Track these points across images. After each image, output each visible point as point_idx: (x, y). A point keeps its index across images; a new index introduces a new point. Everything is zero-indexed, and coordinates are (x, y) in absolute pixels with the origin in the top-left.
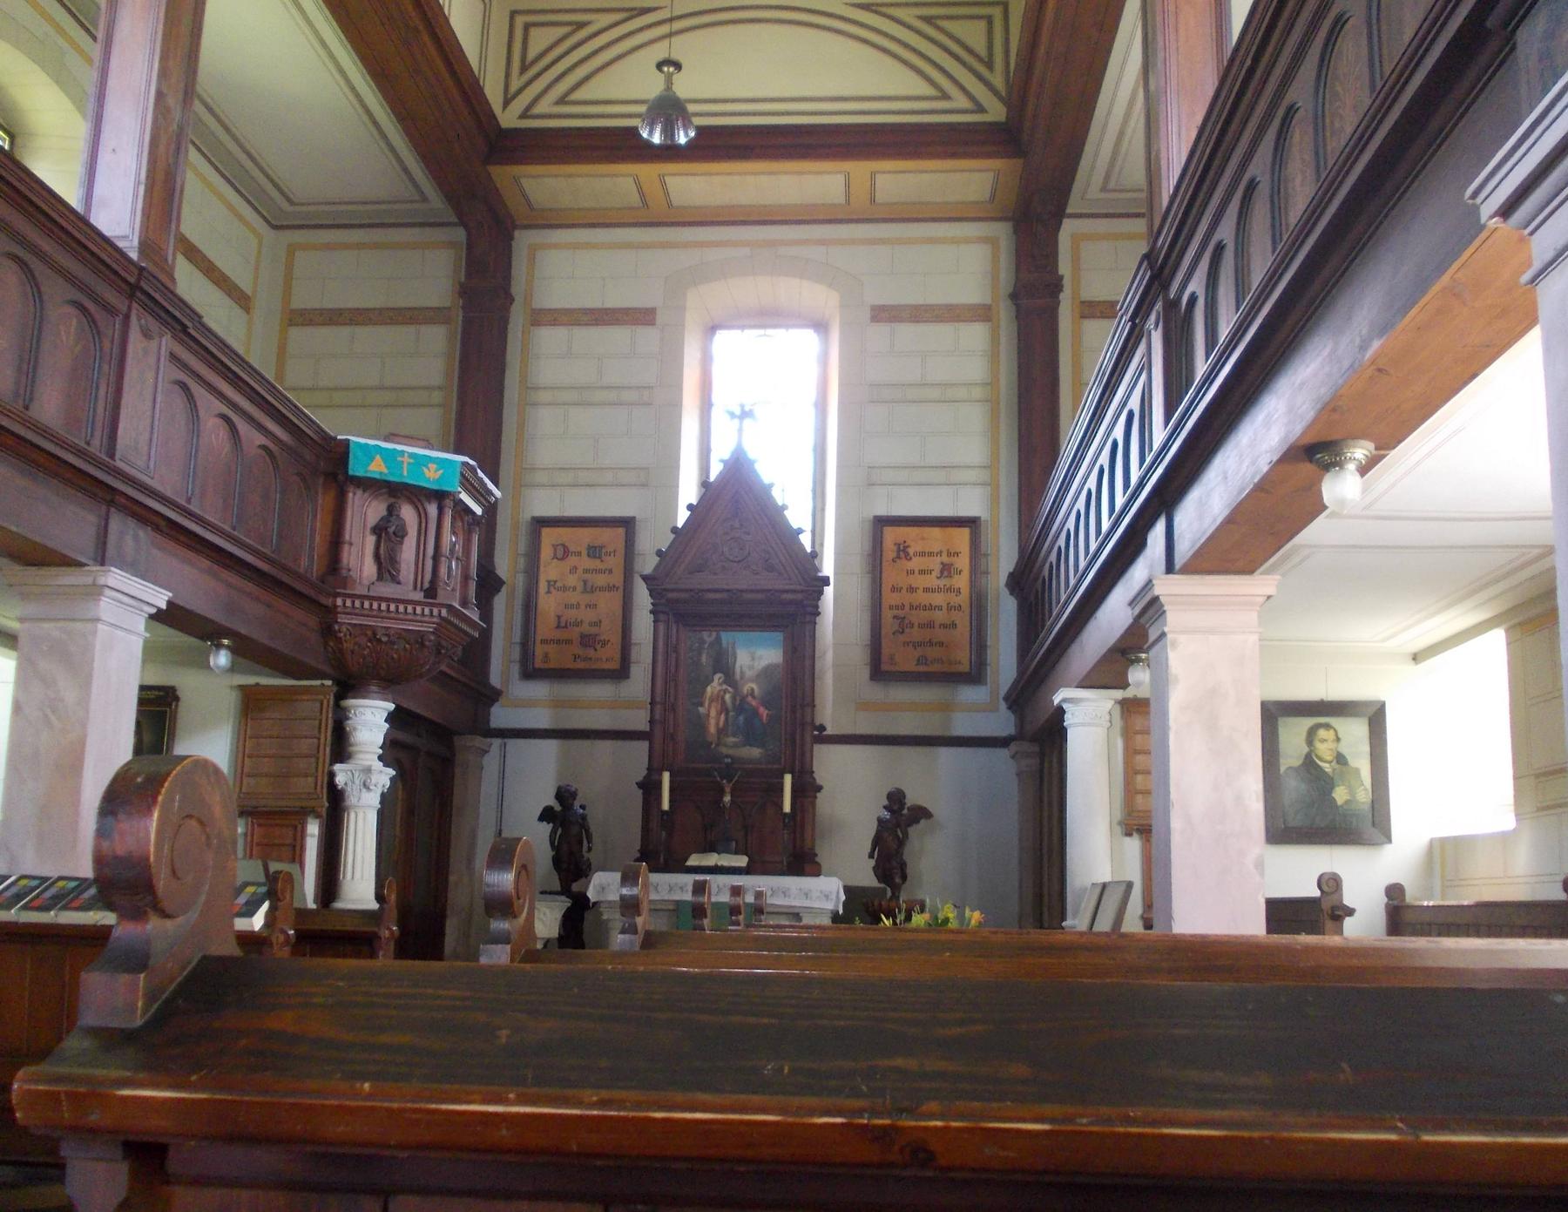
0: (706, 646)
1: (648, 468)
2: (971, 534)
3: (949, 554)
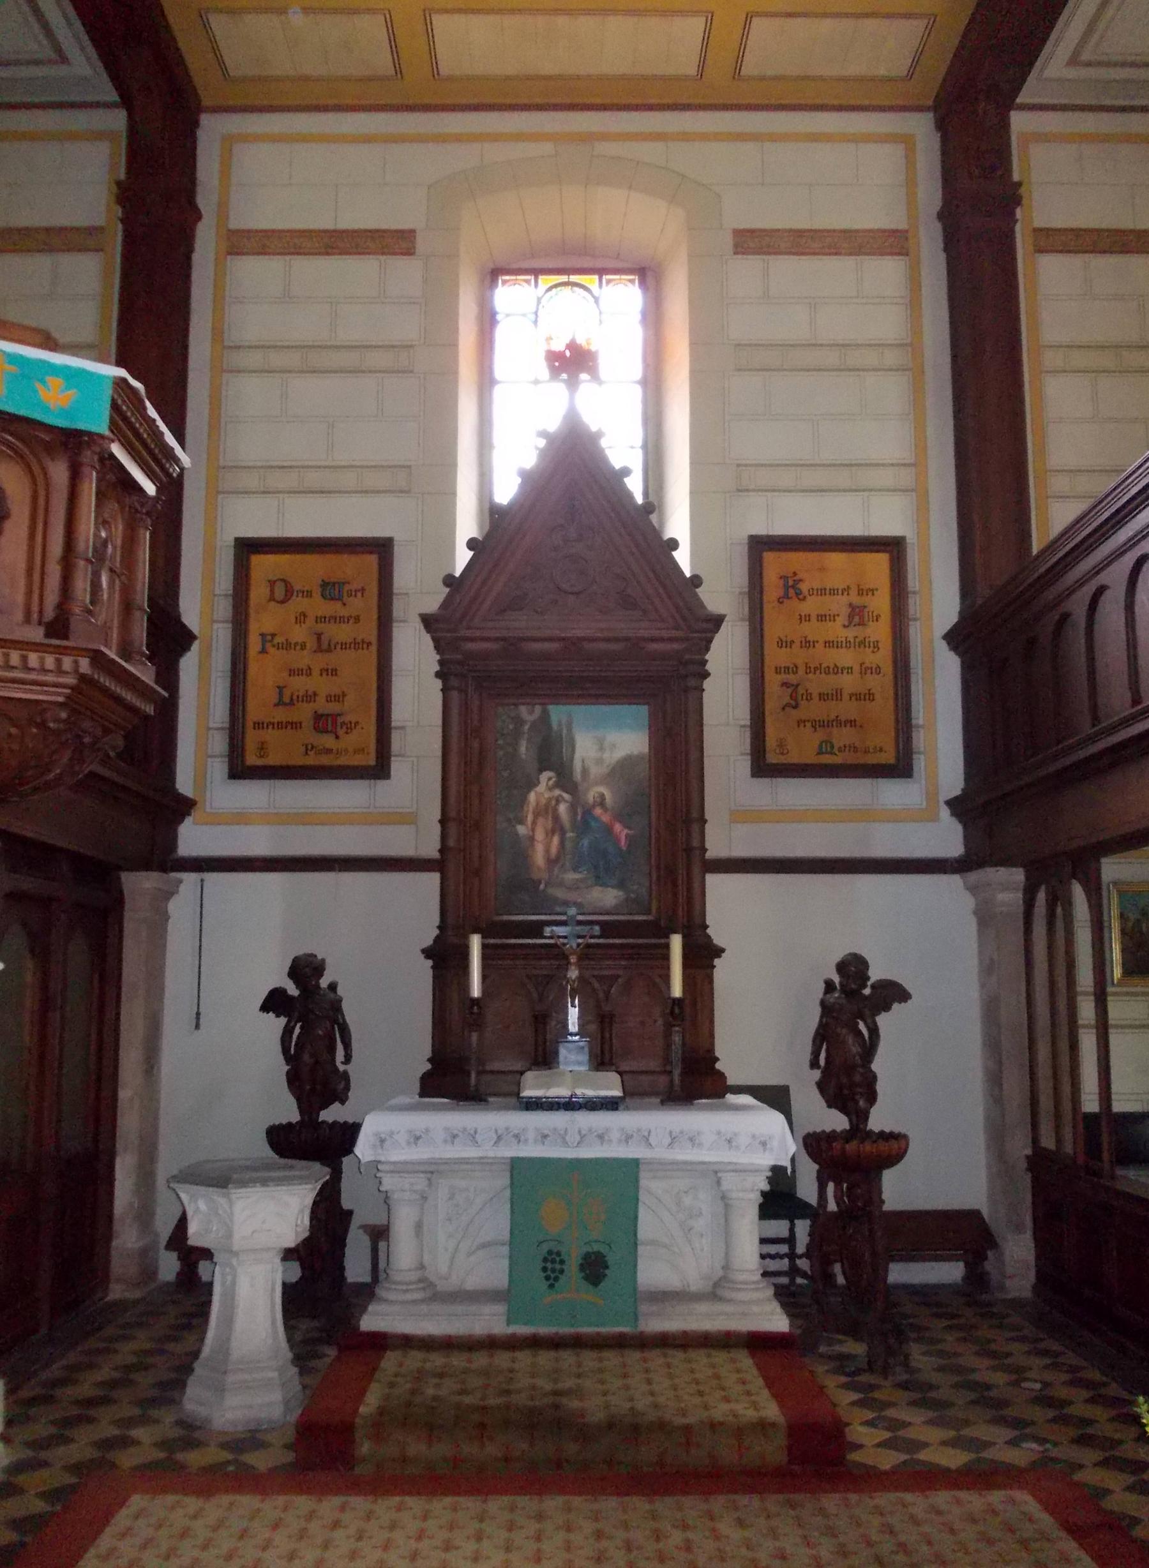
0: (526, 727)
1: (409, 467)
2: (892, 560)
3: (861, 592)
